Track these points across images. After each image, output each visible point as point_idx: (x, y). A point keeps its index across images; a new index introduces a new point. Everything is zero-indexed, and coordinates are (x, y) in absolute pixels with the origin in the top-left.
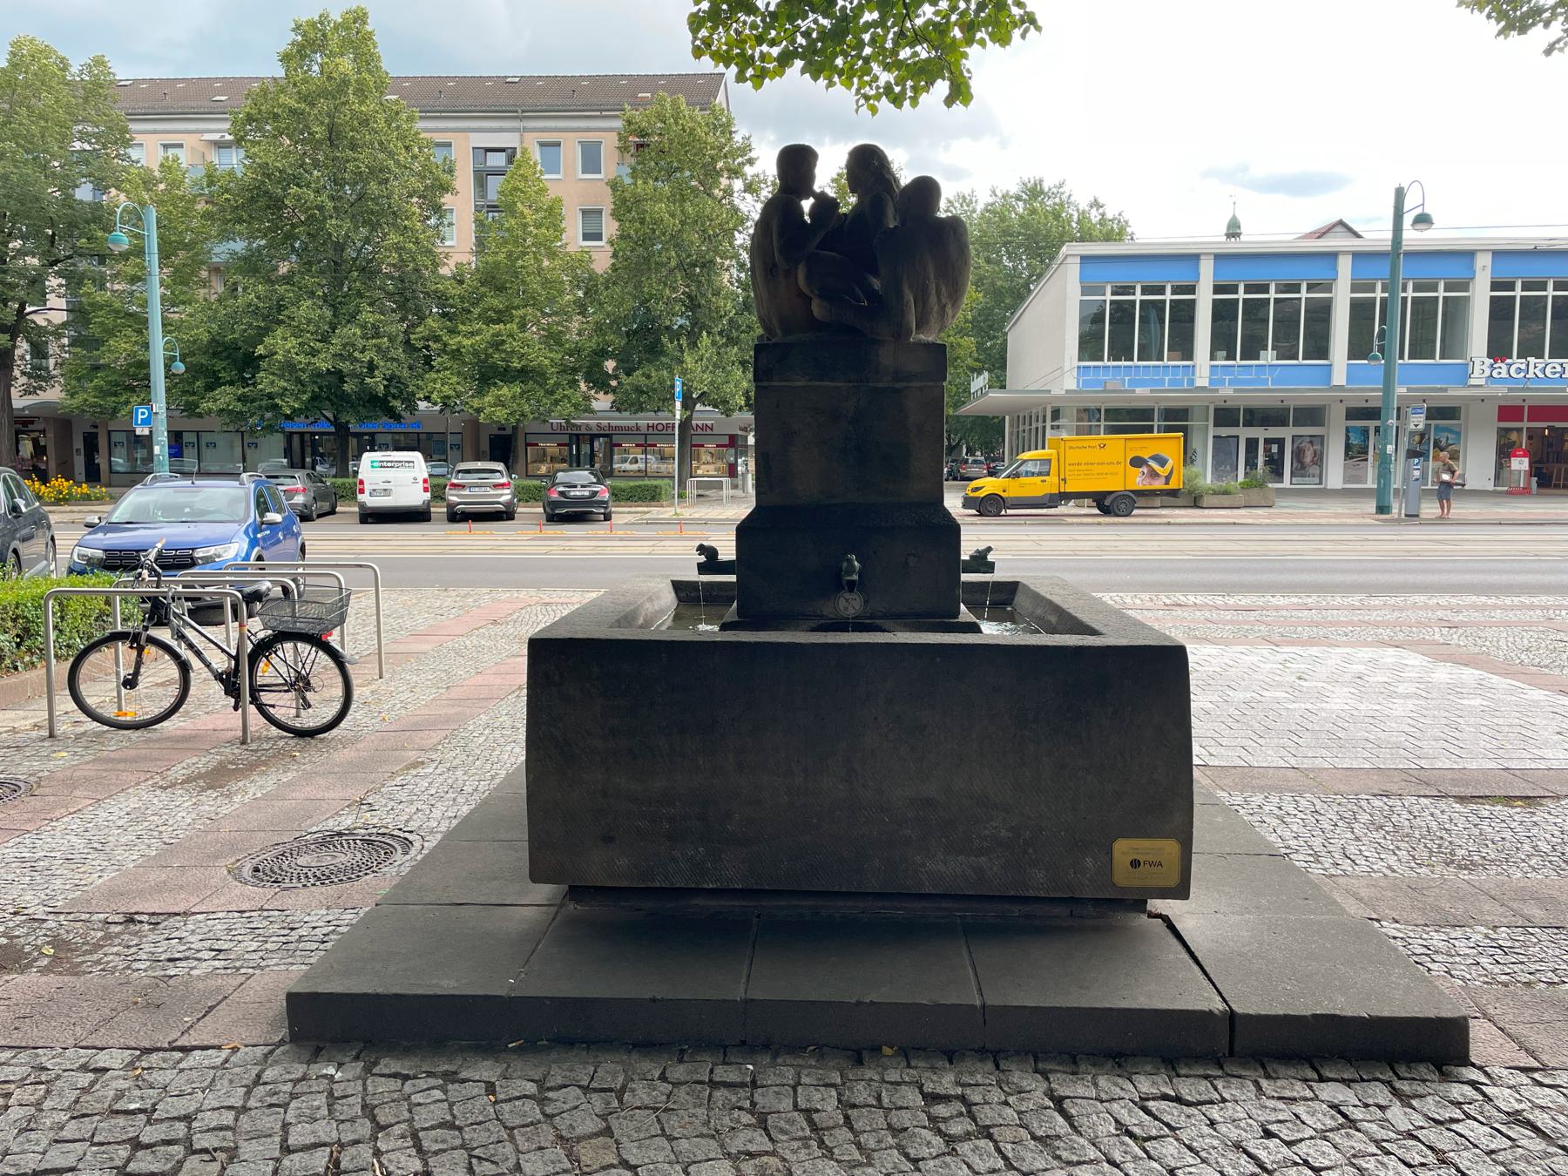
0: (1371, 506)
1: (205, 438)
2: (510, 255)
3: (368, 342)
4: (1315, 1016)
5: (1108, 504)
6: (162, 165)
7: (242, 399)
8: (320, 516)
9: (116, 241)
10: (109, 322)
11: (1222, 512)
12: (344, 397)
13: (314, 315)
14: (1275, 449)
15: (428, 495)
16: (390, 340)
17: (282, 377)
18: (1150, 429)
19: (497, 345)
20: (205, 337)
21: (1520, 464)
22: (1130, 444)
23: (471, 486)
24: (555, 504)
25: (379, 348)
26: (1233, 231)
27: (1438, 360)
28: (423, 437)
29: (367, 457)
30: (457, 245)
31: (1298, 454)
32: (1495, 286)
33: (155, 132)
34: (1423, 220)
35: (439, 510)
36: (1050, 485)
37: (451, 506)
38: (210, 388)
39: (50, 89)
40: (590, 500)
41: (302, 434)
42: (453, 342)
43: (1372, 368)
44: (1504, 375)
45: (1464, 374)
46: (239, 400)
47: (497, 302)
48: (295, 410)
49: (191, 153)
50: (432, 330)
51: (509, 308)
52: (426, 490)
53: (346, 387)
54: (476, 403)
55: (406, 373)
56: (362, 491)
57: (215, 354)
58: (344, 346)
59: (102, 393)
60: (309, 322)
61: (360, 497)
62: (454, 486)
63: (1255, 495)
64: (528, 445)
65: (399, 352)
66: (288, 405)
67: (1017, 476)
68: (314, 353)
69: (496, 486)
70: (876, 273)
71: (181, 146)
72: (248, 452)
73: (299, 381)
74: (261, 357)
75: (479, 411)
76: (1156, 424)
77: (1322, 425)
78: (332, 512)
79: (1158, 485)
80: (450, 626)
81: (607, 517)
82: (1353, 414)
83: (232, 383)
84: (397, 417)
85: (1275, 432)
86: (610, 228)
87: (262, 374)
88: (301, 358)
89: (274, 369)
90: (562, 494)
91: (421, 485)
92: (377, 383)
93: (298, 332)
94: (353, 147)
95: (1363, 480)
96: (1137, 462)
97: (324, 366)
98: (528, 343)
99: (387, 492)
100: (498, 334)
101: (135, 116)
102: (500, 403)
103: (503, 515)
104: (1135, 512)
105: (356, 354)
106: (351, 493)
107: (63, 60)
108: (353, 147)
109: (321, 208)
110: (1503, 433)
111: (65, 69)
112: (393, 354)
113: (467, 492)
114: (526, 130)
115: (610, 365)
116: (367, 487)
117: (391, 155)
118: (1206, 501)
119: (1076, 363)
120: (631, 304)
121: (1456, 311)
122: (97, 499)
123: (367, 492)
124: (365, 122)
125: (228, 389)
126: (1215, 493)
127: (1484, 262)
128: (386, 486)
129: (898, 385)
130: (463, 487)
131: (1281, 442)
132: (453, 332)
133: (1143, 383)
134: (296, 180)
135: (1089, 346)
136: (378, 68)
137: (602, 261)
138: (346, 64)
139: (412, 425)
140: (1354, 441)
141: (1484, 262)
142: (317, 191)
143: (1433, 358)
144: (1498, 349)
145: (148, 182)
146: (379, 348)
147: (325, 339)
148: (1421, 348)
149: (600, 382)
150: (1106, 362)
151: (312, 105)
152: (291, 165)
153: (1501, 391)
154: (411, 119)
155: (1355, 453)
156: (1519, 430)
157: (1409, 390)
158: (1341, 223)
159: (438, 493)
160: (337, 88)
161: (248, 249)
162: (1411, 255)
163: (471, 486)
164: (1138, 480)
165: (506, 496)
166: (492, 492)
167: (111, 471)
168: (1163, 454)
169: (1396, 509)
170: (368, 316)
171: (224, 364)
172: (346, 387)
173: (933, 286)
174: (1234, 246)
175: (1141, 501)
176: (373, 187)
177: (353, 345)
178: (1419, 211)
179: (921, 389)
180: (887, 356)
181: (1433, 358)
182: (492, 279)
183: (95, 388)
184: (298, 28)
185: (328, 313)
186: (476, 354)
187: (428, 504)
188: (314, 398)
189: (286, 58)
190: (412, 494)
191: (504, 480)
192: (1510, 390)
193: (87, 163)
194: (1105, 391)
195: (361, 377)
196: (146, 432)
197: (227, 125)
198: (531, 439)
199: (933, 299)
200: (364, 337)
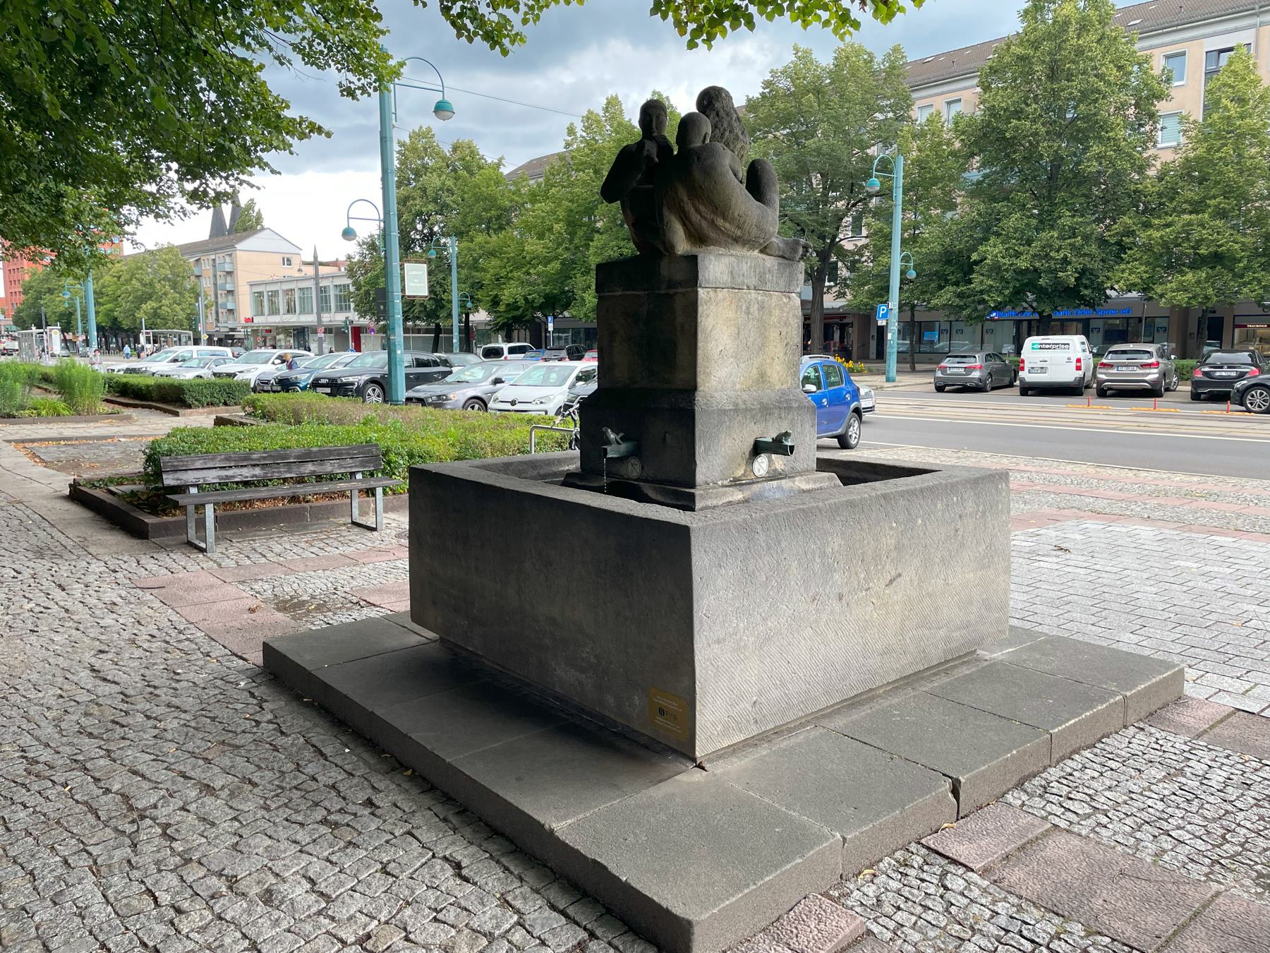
3: (1062, 245)
4: (594, 861)
7: (960, 296)
8: (993, 389)
9: (872, 186)
17: (989, 277)
20: (938, 249)
23: (1119, 365)
24: (1196, 384)
25: (1072, 246)
30: (1168, 146)
33: (942, 93)
38: (941, 288)
50: (1126, 226)
51: (1202, 201)
57: (949, 262)
60: (1016, 230)
64: (1235, 326)
65: (1093, 248)
68: (1018, 255)
69: (1144, 366)
71: (959, 100)
72: (986, 337)
74: (976, 263)
83: (957, 284)
84: (1091, 304)
88: (1006, 261)
89: (984, 271)
90: (1205, 374)
91: (1074, 364)
100: (1190, 224)
101: (917, 87)
102: (1183, 288)
103: (1151, 392)
107: (870, 54)
109: (1036, 134)
111: (871, 61)
112: (1086, 250)
113: (1115, 371)
114: (1262, 24)
116: (1027, 366)
117: (1100, 77)
125: (951, 288)
128: (1043, 365)
129: (672, 291)
130: (1110, 366)
134: (1018, 114)
154: (1131, 42)
163: (1119, 365)
165: (1153, 375)
166: (1139, 371)
170: (1066, 220)
172: (1041, 282)
173: (692, 210)
179: (683, 294)
190: (1068, 375)
195: (1053, 271)
197: (976, 81)
198: (1238, 321)
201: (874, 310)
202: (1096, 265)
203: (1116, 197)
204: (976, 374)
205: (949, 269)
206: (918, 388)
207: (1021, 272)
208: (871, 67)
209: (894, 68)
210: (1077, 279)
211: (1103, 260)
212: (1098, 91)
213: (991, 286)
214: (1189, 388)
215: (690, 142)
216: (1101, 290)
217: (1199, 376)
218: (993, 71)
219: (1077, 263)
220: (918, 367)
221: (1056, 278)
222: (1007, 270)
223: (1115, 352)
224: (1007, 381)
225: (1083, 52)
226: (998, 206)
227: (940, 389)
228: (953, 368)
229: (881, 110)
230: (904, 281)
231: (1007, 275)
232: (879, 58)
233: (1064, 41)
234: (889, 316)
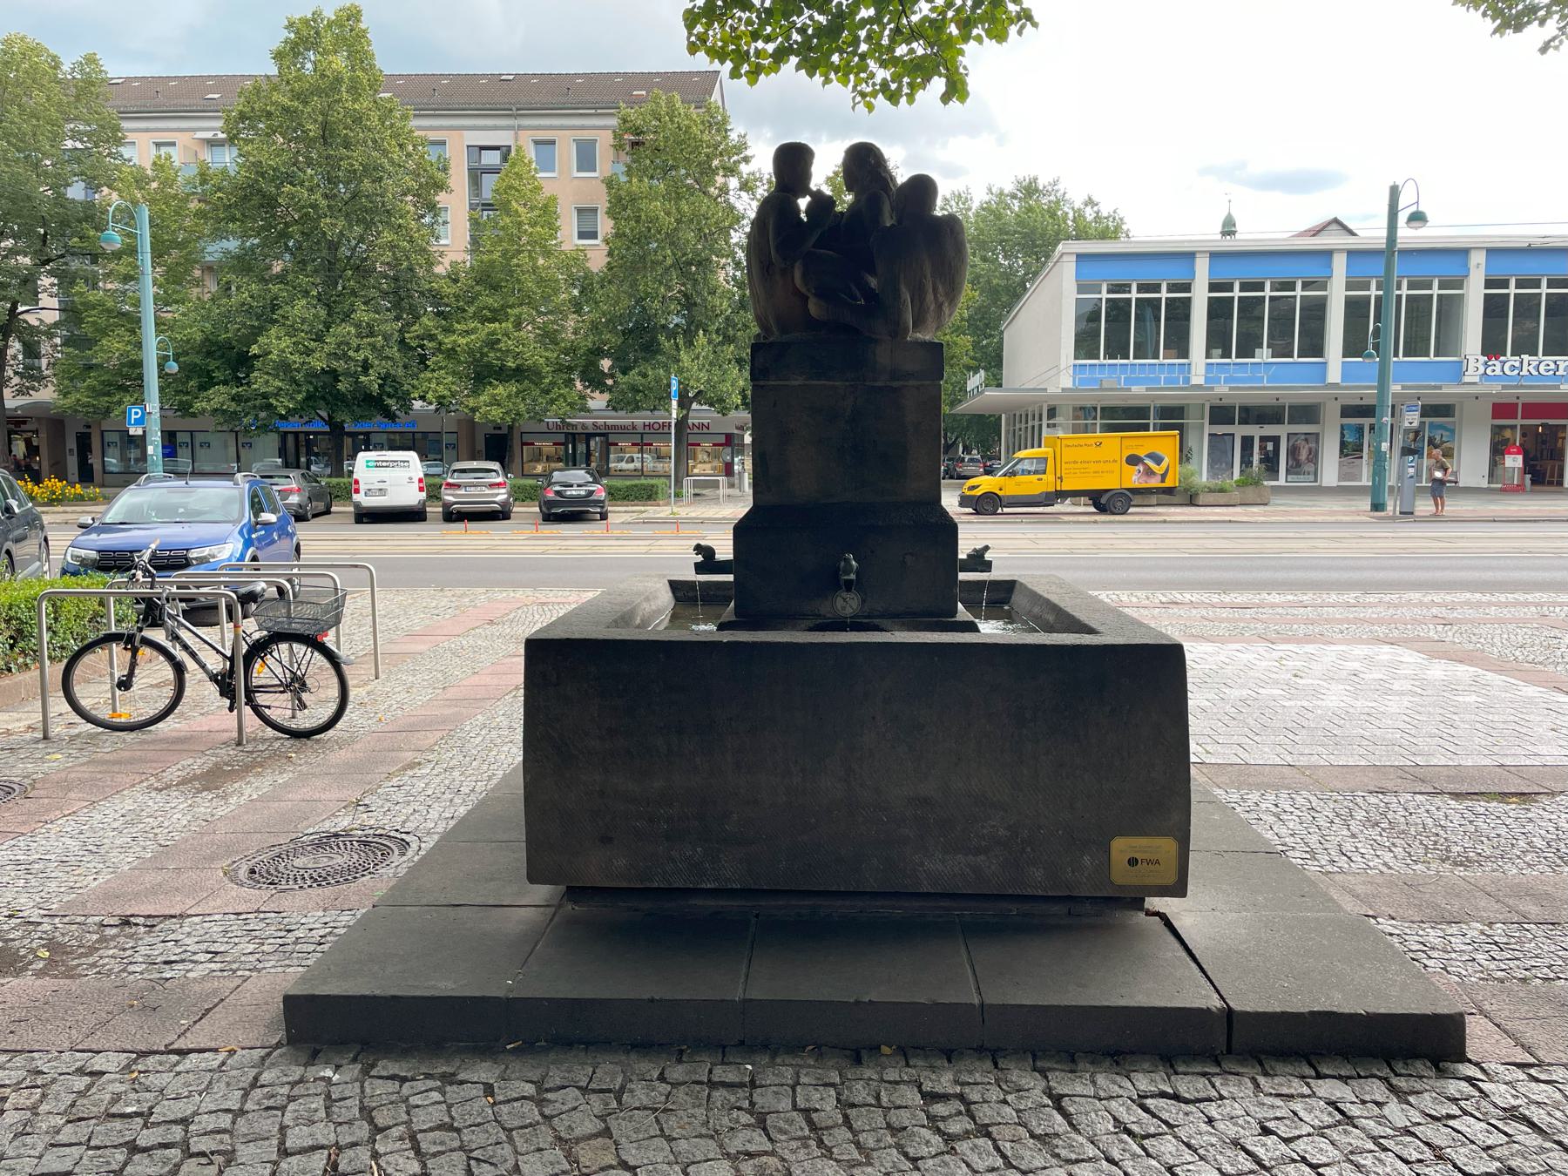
0: (1366, 504)
1: (199, 438)
2: (505, 253)
3: (362, 341)
5: (1105, 502)
6: (154, 164)
8: (315, 516)
9: (109, 240)
10: (102, 322)
11: (1218, 510)
12: (340, 398)
14: (1270, 446)
16: (385, 339)
17: (277, 376)
18: (1146, 428)
19: (492, 344)
20: (198, 337)
21: (1514, 462)
22: (1126, 442)
24: (550, 504)
25: (373, 347)
26: (1229, 229)
31: (1293, 452)
32: (1489, 284)
33: (147, 130)
34: (1417, 218)
35: (434, 509)
36: (1046, 483)
37: (446, 506)
38: (203, 387)
40: (587, 500)
41: (296, 434)
42: (448, 340)
43: (1367, 366)
44: (1498, 372)
45: (1458, 371)
46: (233, 399)
47: (492, 301)
48: (289, 410)
50: (426, 328)
51: (504, 307)
52: (421, 489)
53: (340, 386)
54: (471, 402)
55: (400, 372)
56: (357, 491)
57: (209, 354)
59: (95, 392)
60: (304, 321)
61: (355, 497)
63: (1250, 493)
64: (523, 444)
65: (394, 351)
66: (283, 405)
67: (1014, 474)
68: (308, 352)
69: (492, 486)
71: (173, 144)
73: (294, 381)
74: (256, 357)
75: (474, 410)
76: (1151, 422)
77: (1316, 422)
78: (327, 512)
79: (1154, 483)
80: (447, 626)
81: (604, 517)
82: (1347, 411)
83: (225, 383)
85: (1270, 430)
86: (605, 226)
87: (256, 374)
89: (269, 368)
90: (558, 493)
92: (371, 381)
93: (292, 331)
95: (1358, 477)
96: (1133, 460)
97: (318, 365)
98: (524, 342)
99: (382, 492)
100: (493, 333)
101: (127, 114)
102: (495, 402)
103: (499, 514)
104: (1131, 510)
105: (351, 353)
106: (346, 492)
107: (54, 58)
108: (347, 145)
109: (314, 206)
110: (1497, 430)
111: (56, 67)
113: (462, 492)
114: (520, 128)
115: (606, 364)
116: (362, 487)
117: (385, 153)
118: (1201, 499)
119: (1072, 361)
120: (627, 302)
121: (1451, 308)
122: (91, 499)
124: (358, 120)
125: (222, 388)
126: (1211, 491)
127: (1478, 260)
128: (381, 486)
129: (895, 384)
130: (458, 486)
131: (1276, 440)
132: (448, 331)
133: (1137, 381)
134: (290, 179)
135: (1085, 344)
136: (372, 66)
137: (597, 258)
138: (339, 62)
140: (1348, 439)
141: (1478, 260)
142: (311, 190)
144: (1492, 347)
145: (140, 180)
146: (373, 347)
147: (319, 338)
149: (596, 381)
150: (1234, 359)
151: (306, 103)
152: (284, 164)
153: (1495, 388)
154: (405, 117)
155: (1350, 450)
156: (1513, 427)
157: (1403, 388)
158: (1336, 221)
159: (433, 492)
160: (329, 86)
162: (1407, 253)
164: (1133, 478)
165: (502, 495)
167: (104, 472)
168: (1160, 453)
169: (1391, 506)
170: (363, 315)
171: (217, 363)
172: (340, 386)
174: (1228, 244)
175: (1137, 500)
178: (1413, 209)
182: (486, 278)
184: (291, 25)
185: (323, 313)
186: (471, 352)
187: (424, 504)
189: (278, 56)
190: (410, 496)
191: (500, 480)
194: (1101, 389)
195: (355, 375)
196: (140, 432)
197: (220, 124)
198: (526, 438)
200: (359, 335)
202: (400, 372)
203: (402, 293)
205: (213, 364)
207: (312, 375)
211: (405, 367)
212: (384, 170)
214: (537, 509)
215: (893, 179)
216: (405, 400)
217: (551, 496)
219: (380, 367)
221: (357, 382)
223: (464, 471)
224: (321, 506)
230: (162, 374)
231: (299, 376)
233: (338, 101)
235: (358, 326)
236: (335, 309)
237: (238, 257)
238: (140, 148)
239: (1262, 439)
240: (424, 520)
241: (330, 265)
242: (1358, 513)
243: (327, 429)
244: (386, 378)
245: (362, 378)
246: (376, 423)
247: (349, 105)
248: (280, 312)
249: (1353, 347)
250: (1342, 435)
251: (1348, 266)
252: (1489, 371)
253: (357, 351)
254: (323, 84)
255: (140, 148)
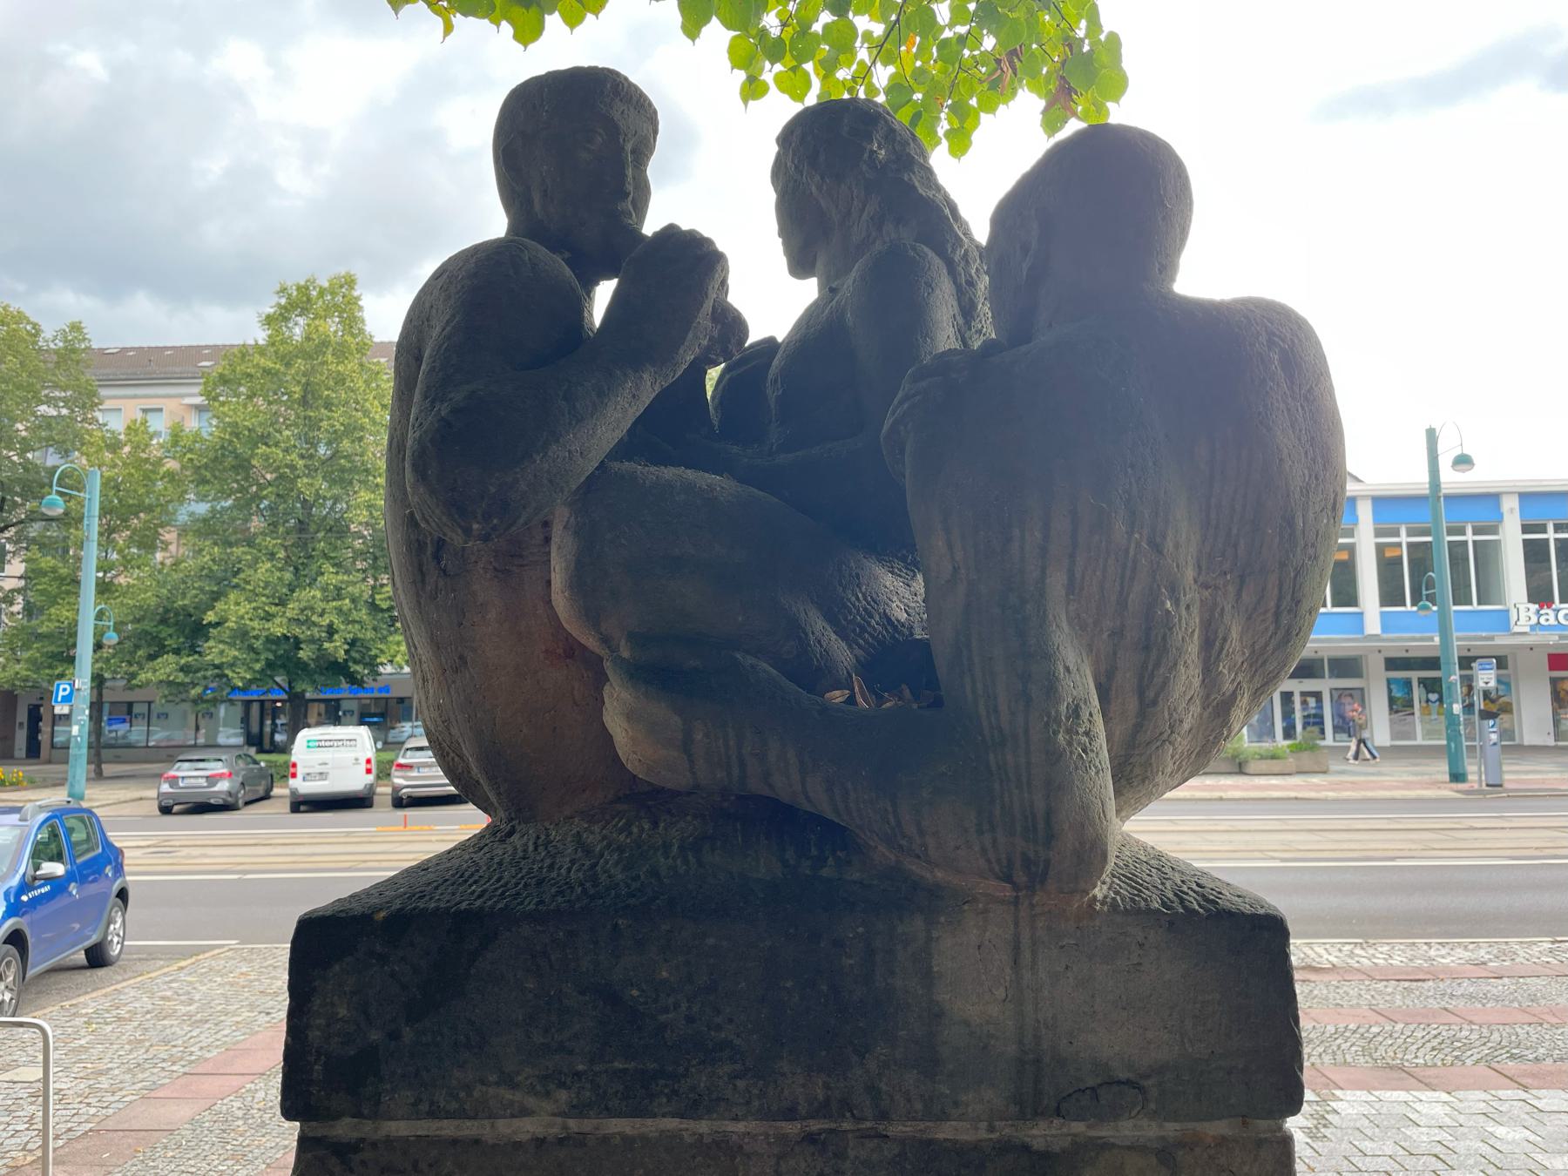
0: (1441, 769)
6: (129, 428)
7: (185, 669)
8: (247, 803)
10: (53, 589)
11: (1274, 781)
12: (302, 666)
13: (274, 579)
15: (371, 778)
16: (353, 601)
20: (153, 601)
25: (340, 611)
27: (1475, 606)
28: (393, 703)
29: (304, 735)
32: (1526, 529)
33: (135, 397)
34: (1463, 461)
35: (384, 790)
37: (396, 789)
38: (152, 657)
39: (16, 354)
41: (262, 702)
44: (1552, 621)
46: (182, 669)
49: (174, 415)
52: (369, 771)
53: (301, 654)
55: (370, 634)
56: (294, 775)
58: (302, 611)
59: (35, 665)
60: (267, 584)
61: (292, 782)
62: (400, 766)
63: (1306, 759)
65: (363, 614)
66: (239, 677)
68: (268, 617)
70: (900, 549)
71: (160, 410)
73: (251, 649)
74: (210, 624)
78: (266, 797)
82: (1392, 664)
83: (177, 652)
85: (1310, 685)
87: (211, 643)
88: (255, 624)
89: (226, 635)
91: (363, 766)
92: (337, 648)
94: (328, 405)
95: (1411, 735)
97: (279, 631)
99: (322, 776)
105: (314, 618)
107: (35, 325)
108: (328, 405)
109: (293, 467)
111: (37, 335)
112: (355, 615)
113: (415, 774)
116: (300, 771)
117: (366, 413)
118: (1252, 767)
121: (1488, 555)
122: (12, 784)
123: (300, 776)
124: (341, 380)
125: (171, 658)
126: (1262, 758)
127: (1510, 506)
129: (1043, 1134)
131: (1318, 696)
134: (264, 439)
136: (361, 331)
138: (332, 326)
139: (380, 690)
140: (1397, 694)
141: (1510, 506)
142: (286, 451)
143: (1471, 603)
144: (1539, 595)
145: (114, 446)
146: (340, 611)
147: (282, 603)
148: (1461, 597)
151: (288, 365)
152: (261, 424)
153: (1552, 639)
155: (1399, 705)
157: (1561, 637)
159: (384, 773)
160: (316, 348)
161: (213, 510)
162: (1452, 498)
167: (53, 746)
170: (331, 577)
171: (170, 631)
172: (301, 654)
176: (346, 444)
177: (312, 609)
178: (1458, 452)
180: (974, 976)
181: (1471, 603)
183: (28, 660)
184: (283, 290)
185: (288, 576)
187: (371, 789)
188: (270, 665)
189: (269, 321)
190: (354, 780)
192: (1561, 637)
193: (49, 427)
196: (66, 710)
197: (196, 390)
199: (1187, 679)
200: (326, 600)
201: (47, 696)
204: (223, 786)
205: (165, 631)
206: (127, 810)
207: (271, 641)
208: (36, 343)
209: (74, 351)
210: (347, 652)
211: (375, 629)
212: (362, 428)
213: (235, 658)
216: (372, 665)
218: (224, 380)
219: (346, 632)
220: (108, 769)
222: (256, 638)
224: (261, 791)
225: (343, 381)
226: (238, 551)
227: (166, 810)
228: (191, 776)
229: (49, 401)
231: (258, 644)
232: (48, 332)
234: (73, 698)
235: (324, 589)
236: (301, 570)
237: (205, 521)
238: (117, 413)
239: (1303, 694)
240: (371, 806)
241: (302, 526)
242: (1435, 784)
243: (285, 697)
244: (353, 643)
245: (326, 645)
246: (344, 690)
247: (333, 367)
248: (242, 576)
249: (1391, 595)
250: (1390, 691)
251: (1375, 512)
252: (1542, 620)
253: (321, 615)
254: (309, 347)
255: (117, 413)
